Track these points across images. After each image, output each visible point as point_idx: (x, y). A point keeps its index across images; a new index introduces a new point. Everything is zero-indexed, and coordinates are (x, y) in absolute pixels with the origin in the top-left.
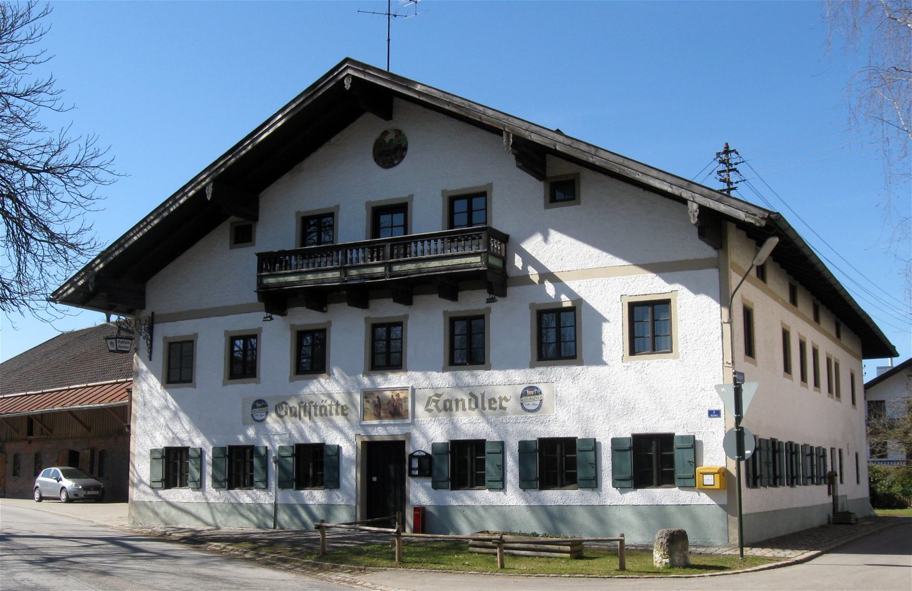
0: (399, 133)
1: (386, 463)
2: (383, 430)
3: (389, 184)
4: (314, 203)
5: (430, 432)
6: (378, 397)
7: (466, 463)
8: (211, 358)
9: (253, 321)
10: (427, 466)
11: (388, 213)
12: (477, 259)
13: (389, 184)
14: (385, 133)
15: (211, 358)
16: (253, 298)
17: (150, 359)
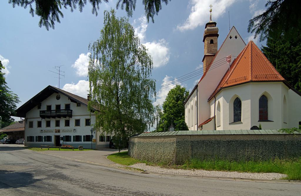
0: (59, 95)
1: (58, 138)
2: (58, 134)
3: (58, 102)
4: (49, 104)
5: (62, 135)
7: (68, 138)
8: (35, 124)
9: (40, 119)
10: (62, 139)
11: (58, 107)
12: (66, 113)
13: (58, 102)
14: (58, 95)
15: (35, 124)
16: (39, 117)
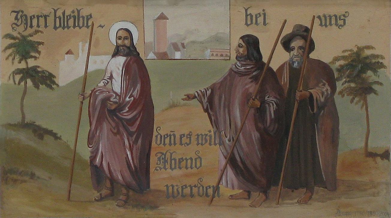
6: (127, 49)
17: (285, 21)
